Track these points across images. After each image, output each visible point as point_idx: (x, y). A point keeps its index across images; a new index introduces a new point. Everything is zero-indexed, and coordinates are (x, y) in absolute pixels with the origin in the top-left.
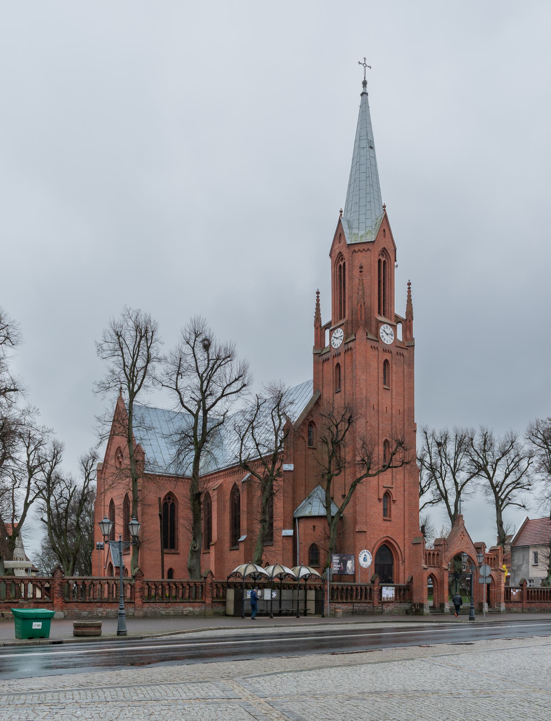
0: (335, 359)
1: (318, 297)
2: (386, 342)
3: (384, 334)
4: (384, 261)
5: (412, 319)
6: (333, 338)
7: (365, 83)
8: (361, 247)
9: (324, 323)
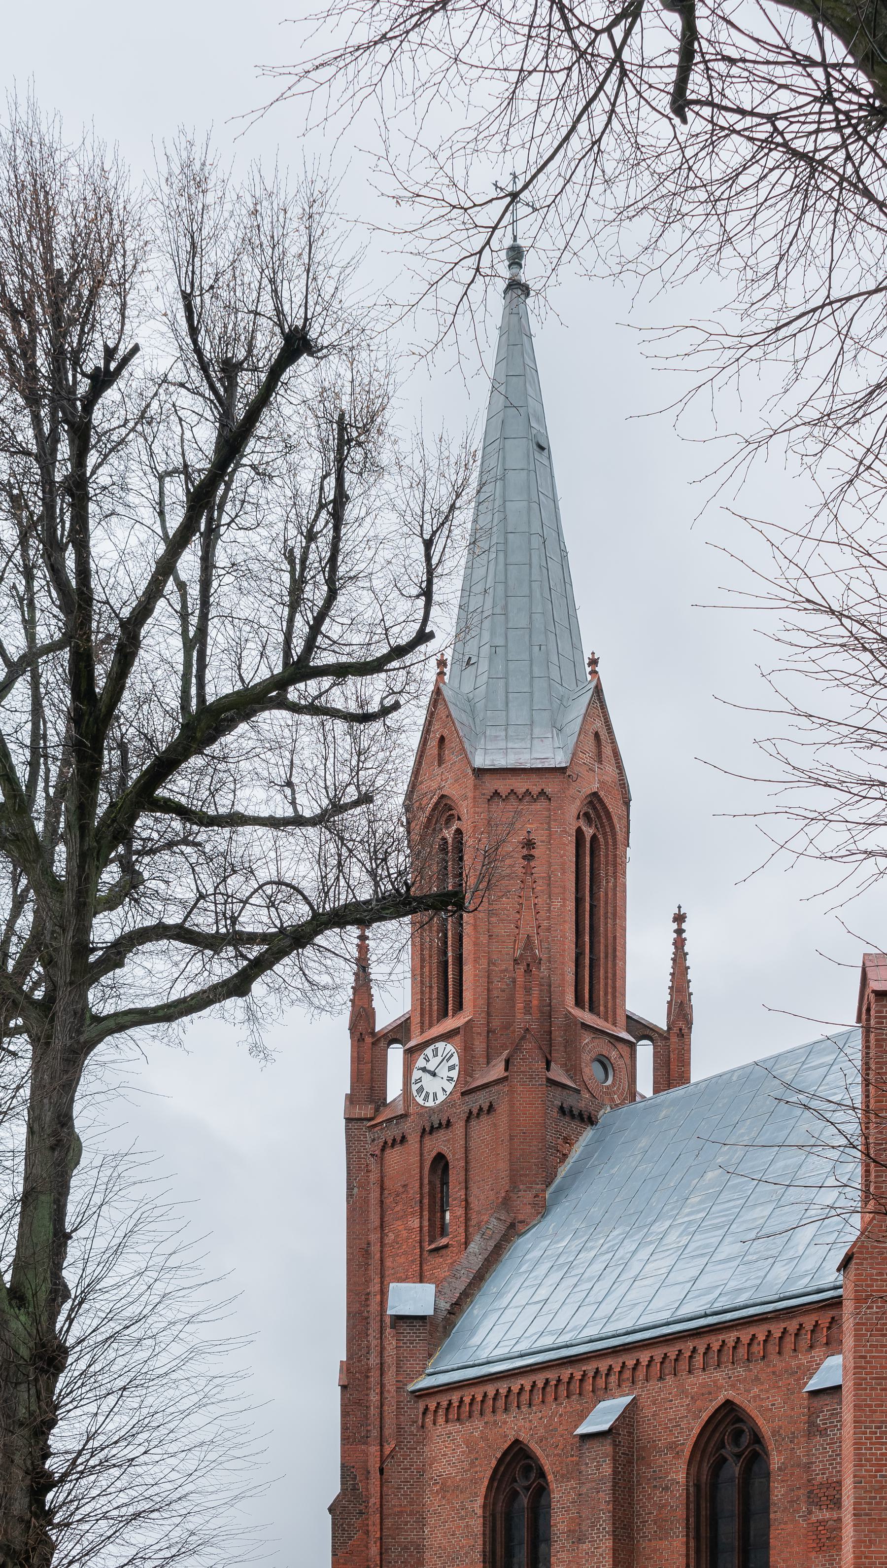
0: (428, 1142)
4: (594, 838)
5: (689, 1023)
6: (416, 1074)
8: (521, 785)
9: (383, 1021)
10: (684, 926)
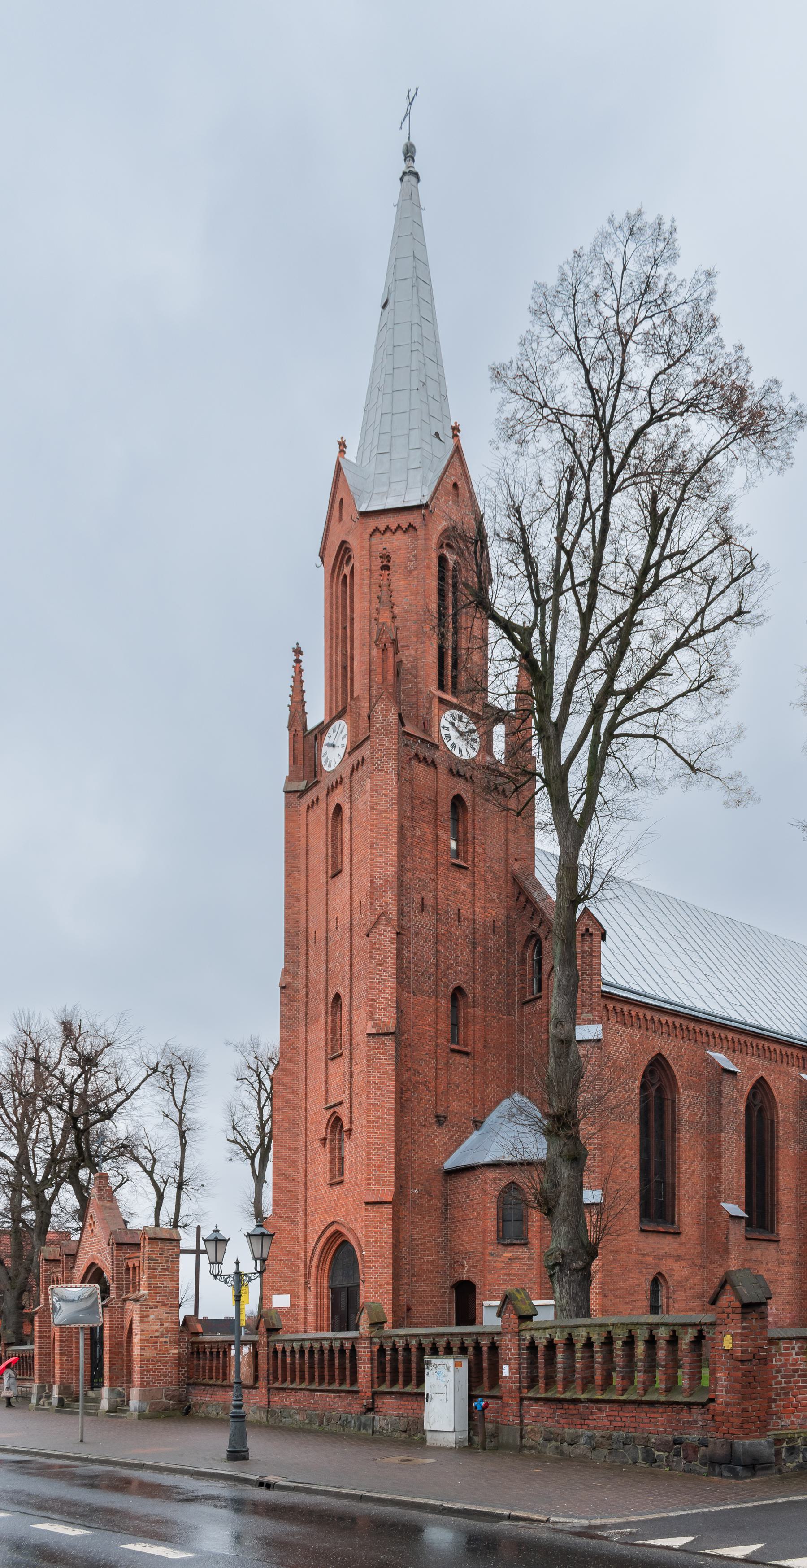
1: (298, 661)
2: (456, 752)
3: (453, 733)
7: (409, 153)
10: (301, 657)
